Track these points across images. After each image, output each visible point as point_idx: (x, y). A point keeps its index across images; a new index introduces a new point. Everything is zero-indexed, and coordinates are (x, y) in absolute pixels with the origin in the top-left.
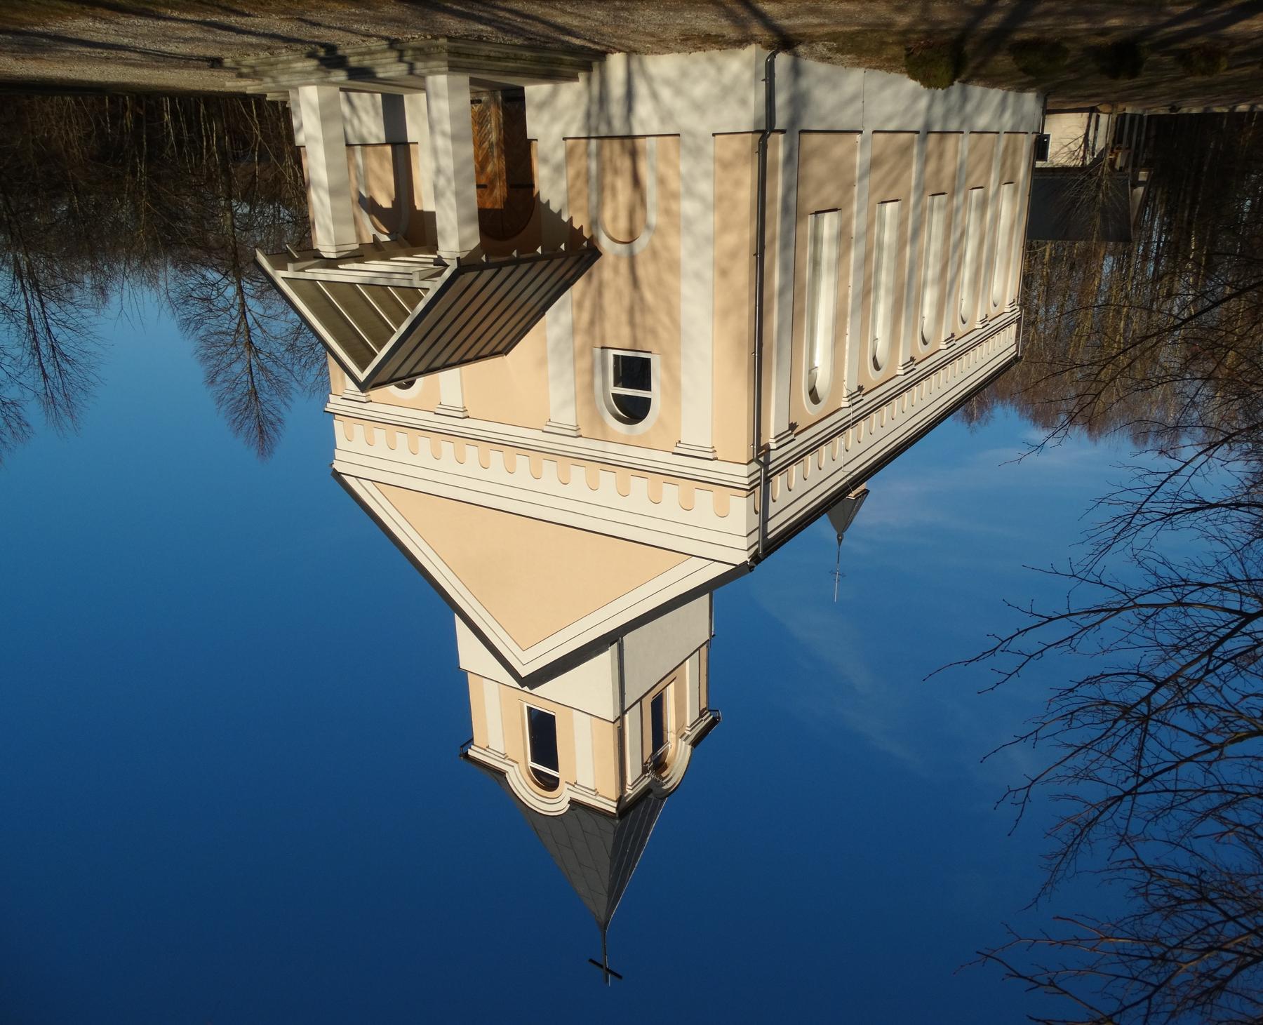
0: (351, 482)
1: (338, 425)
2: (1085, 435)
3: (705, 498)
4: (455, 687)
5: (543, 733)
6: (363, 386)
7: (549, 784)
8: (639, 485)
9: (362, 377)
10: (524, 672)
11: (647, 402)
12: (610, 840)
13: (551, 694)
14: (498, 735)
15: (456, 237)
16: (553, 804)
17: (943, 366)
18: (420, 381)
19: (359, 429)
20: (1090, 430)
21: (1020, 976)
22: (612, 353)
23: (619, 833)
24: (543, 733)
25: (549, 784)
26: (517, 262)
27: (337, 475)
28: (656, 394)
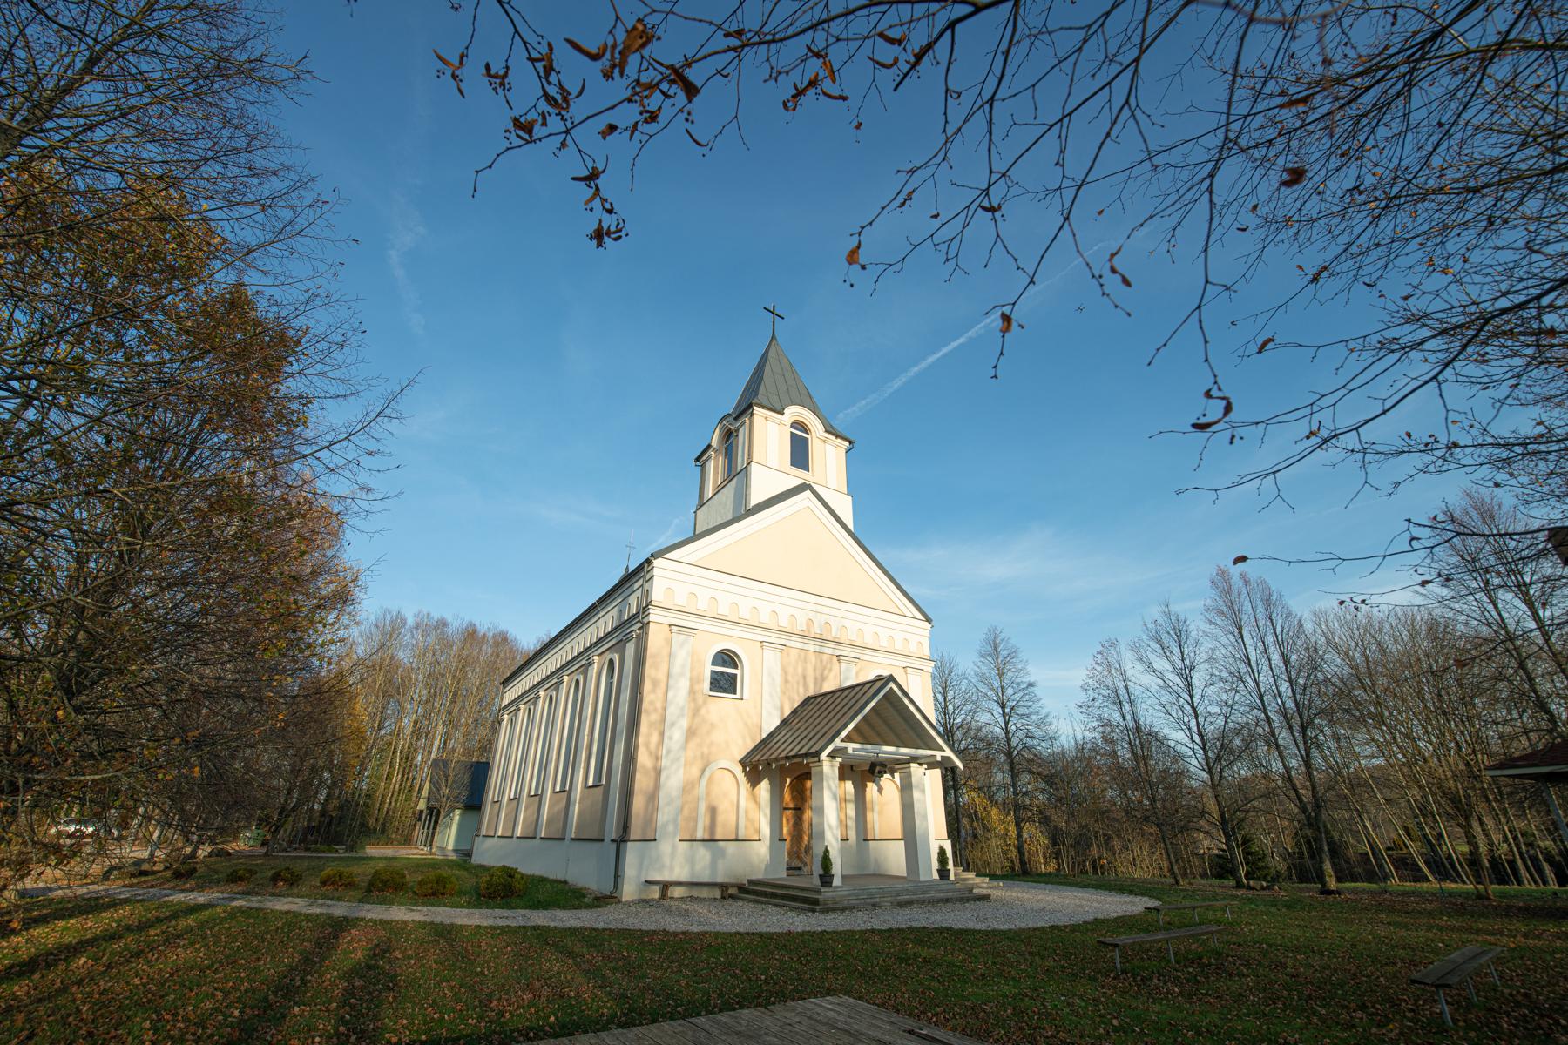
0: (919, 616)
1: (927, 652)
2: (478, 627)
3: (680, 601)
4: (854, 488)
5: (800, 454)
6: (891, 678)
7: (798, 424)
8: (724, 610)
9: (892, 685)
10: (808, 492)
11: (714, 663)
12: (762, 390)
13: (796, 477)
14: (829, 456)
15: (829, 768)
16: (794, 412)
17: (543, 680)
18: (871, 678)
19: (914, 650)
20: (475, 631)
21: (1107, 14)
22: (892, 685)
23: (756, 395)
24: (800, 454)
25: (798, 424)
26: (787, 758)
27: (929, 620)
28: (708, 669)
